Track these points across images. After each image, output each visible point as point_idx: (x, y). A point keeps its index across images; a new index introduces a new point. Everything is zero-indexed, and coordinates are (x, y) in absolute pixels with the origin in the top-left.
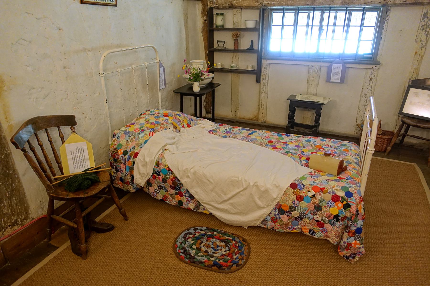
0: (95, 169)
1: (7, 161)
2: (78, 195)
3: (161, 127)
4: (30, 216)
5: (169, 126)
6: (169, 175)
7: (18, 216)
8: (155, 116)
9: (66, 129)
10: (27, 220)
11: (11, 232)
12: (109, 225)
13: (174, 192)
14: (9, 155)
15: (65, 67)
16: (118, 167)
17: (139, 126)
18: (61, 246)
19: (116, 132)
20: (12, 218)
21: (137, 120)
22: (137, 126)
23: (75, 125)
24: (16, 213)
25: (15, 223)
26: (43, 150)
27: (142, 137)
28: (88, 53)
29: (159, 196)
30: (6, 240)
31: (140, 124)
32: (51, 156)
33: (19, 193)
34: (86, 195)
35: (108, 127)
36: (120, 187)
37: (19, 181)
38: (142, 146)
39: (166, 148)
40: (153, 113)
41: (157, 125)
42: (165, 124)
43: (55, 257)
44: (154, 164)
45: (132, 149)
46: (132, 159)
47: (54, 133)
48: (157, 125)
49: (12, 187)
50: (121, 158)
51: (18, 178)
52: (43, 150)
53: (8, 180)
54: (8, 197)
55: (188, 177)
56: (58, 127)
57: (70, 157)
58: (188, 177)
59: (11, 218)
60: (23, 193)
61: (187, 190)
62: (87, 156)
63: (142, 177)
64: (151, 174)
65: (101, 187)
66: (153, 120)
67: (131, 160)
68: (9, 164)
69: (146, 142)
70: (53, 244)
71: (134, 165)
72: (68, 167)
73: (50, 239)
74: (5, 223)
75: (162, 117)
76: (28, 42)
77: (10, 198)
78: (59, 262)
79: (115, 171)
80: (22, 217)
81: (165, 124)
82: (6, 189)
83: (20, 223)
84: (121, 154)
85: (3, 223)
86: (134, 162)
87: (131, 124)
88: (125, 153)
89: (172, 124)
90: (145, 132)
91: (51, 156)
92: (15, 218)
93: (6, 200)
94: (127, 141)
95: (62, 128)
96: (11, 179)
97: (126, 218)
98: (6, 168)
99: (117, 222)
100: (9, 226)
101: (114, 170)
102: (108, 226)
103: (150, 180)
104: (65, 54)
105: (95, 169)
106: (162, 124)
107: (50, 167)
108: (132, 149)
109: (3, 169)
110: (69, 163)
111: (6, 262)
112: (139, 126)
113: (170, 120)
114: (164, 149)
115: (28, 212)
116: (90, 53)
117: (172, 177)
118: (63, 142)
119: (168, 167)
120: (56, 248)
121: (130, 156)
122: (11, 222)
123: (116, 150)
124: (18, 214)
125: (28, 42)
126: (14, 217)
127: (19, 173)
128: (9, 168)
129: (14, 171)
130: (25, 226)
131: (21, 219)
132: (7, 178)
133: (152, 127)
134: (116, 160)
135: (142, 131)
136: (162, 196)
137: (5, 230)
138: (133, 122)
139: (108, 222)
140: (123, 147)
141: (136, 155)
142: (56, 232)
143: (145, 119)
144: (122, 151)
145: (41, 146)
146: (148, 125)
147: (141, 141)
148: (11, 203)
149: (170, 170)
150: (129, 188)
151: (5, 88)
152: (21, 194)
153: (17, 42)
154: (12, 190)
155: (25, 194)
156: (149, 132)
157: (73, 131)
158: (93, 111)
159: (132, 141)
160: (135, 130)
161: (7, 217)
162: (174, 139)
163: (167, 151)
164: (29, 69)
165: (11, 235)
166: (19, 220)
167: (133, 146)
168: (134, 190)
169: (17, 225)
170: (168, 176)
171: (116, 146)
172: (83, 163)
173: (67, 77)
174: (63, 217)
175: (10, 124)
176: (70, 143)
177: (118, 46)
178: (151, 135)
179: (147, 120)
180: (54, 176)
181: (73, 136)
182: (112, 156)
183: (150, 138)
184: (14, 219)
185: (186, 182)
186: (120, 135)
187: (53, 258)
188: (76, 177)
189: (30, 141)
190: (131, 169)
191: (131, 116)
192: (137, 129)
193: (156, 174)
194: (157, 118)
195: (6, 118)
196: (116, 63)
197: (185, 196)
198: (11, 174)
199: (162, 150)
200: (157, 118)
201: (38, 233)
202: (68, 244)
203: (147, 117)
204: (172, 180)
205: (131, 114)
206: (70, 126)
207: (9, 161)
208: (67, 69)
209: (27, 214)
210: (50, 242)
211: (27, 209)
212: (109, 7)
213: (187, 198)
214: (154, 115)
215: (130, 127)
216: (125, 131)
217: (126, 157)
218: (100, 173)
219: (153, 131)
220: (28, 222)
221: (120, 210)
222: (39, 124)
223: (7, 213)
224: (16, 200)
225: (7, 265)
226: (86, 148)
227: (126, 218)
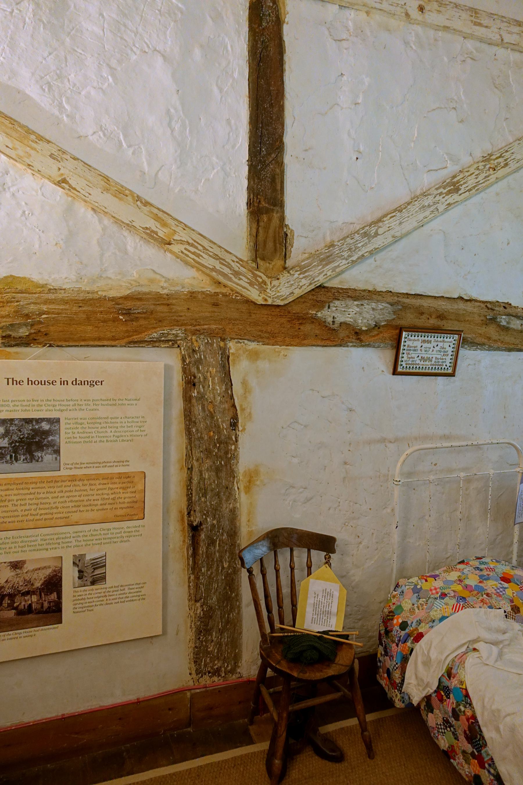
0: (338, 636)
1: (233, 578)
2: (291, 670)
3: (482, 601)
4: (238, 670)
5: (504, 602)
6: (465, 707)
7: (224, 663)
8: (481, 573)
9: (318, 556)
10: (232, 675)
11: (208, 682)
12: (335, 748)
13: (469, 748)
14: (238, 571)
15: (345, 463)
16: (388, 646)
17: (442, 585)
18: (260, 742)
19: (402, 582)
20: (216, 662)
21: (445, 571)
22: (438, 583)
23: (332, 553)
24: (222, 658)
25: (217, 672)
26: (278, 577)
27: (439, 608)
28: (387, 444)
29: (444, 742)
30: (198, 691)
31: (446, 582)
32: (286, 590)
33: (235, 630)
34: (302, 676)
35: (392, 570)
36: (384, 685)
37: (239, 613)
38: (435, 624)
39: (476, 646)
40: (482, 567)
41: (475, 592)
42: (494, 596)
43: (241, 757)
44: (443, 670)
45: (414, 625)
46: (410, 642)
47: (301, 555)
48: (475, 592)
49: (228, 617)
50: (394, 633)
51: (239, 607)
52: (278, 577)
53: (227, 606)
54: (220, 629)
55: (498, 730)
56: (309, 551)
57: (311, 601)
58: (498, 730)
59: (215, 661)
60: (239, 631)
61: (492, 759)
62: (334, 609)
63: (418, 685)
64: (435, 688)
65: (331, 671)
66: (472, 581)
67: (409, 644)
68: (234, 583)
69: (443, 619)
70: (252, 733)
71: (411, 654)
72: (303, 616)
73: (252, 722)
74: (205, 665)
75: (496, 580)
76: (303, 426)
77: (221, 632)
78: (242, 769)
79: (383, 653)
80: (228, 666)
81: (494, 596)
82: (221, 617)
83: (223, 675)
84: (396, 624)
85: (203, 664)
86: (412, 650)
87: (430, 576)
88: (404, 626)
89: (512, 601)
90: (447, 599)
91: (286, 590)
92: (219, 665)
93: (216, 633)
94: (413, 605)
95: (313, 552)
96: (231, 605)
97: (370, 753)
98: (230, 587)
99: (353, 750)
100: (209, 672)
101: (381, 649)
102: (333, 751)
103: (432, 699)
104: (350, 444)
105: (338, 636)
106: (488, 595)
107: (280, 607)
108: (414, 625)
109: (225, 588)
110: (307, 610)
111: (189, 725)
112: (442, 585)
113: (510, 590)
114: (471, 647)
115: (238, 663)
116: (391, 446)
117: (469, 713)
118: (309, 574)
119: (466, 690)
120: (251, 742)
121: (409, 635)
122: (212, 668)
123: (391, 615)
124: (224, 660)
125: (303, 426)
126: (219, 661)
127: (243, 600)
128: (232, 589)
129: (237, 595)
130: (228, 682)
131: (225, 669)
132: (226, 602)
133: (465, 594)
134: (388, 632)
135: (444, 595)
136: (447, 746)
137: (202, 676)
138: (437, 573)
139: (340, 743)
140: (403, 614)
141: (419, 637)
142: (265, 715)
143: (459, 574)
144: (400, 621)
145: (277, 571)
146: (459, 588)
147: (435, 614)
148: (221, 639)
149: (467, 695)
150: (394, 696)
151: (258, 483)
152: (236, 631)
153: (288, 426)
154: (228, 622)
155: (241, 633)
156: (454, 602)
157: (328, 562)
158: (374, 535)
159: (421, 608)
160: (431, 590)
161: (211, 658)
162: (504, 633)
163: (476, 654)
164: (295, 461)
165: (206, 687)
166: (223, 669)
167: (418, 619)
168: (403, 706)
169: (219, 675)
170: (463, 709)
171: (393, 607)
172: (326, 618)
173: (344, 478)
174: (271, 694)
175: (250, 530)
176: (316, 579)
177: (446, 437)
178: (456, 609)
179: (462, 578)
180: (281, 624)
181: (325, 568)
182: (383, 622)
183: (451, 615)
184: (218, 664)
185: (492, 738)
186: (405, 589)
187: (239, 757)
188: (306, 637)
189: (264, 559)
190: (405, 660)
191: (449, 560)
192: (436, 589)
193: (443, 690)
194: (483, 579)
195: (249, 521)
196: (435, 465)
197: (489, 772)
198: (233, 598)
199: (466, 646)
200: (483, 579)
201: (240, 703)
202: (265, 746)
203: (465, 571)
204: (468, 720)
205: (449, 554)
206: (325, 553)
207: (235, 580)
208: (348, 466)
209: (236, 666)
210: (250, 727)
211: (237, 658)
212: (439, 378)
213: (492, 778)
214: (481, 570)
215: (426, 581)
216: (416, 585)
217: (403, 633)
218: (344, 646)
219: (462, 602)
220: (233, 678)
221: (363, 731)
222: (279, 539)
223: (212, 651)
224: (227, 638)
225: (189, 729)
226: (336, 594)
227: (370, 753)
